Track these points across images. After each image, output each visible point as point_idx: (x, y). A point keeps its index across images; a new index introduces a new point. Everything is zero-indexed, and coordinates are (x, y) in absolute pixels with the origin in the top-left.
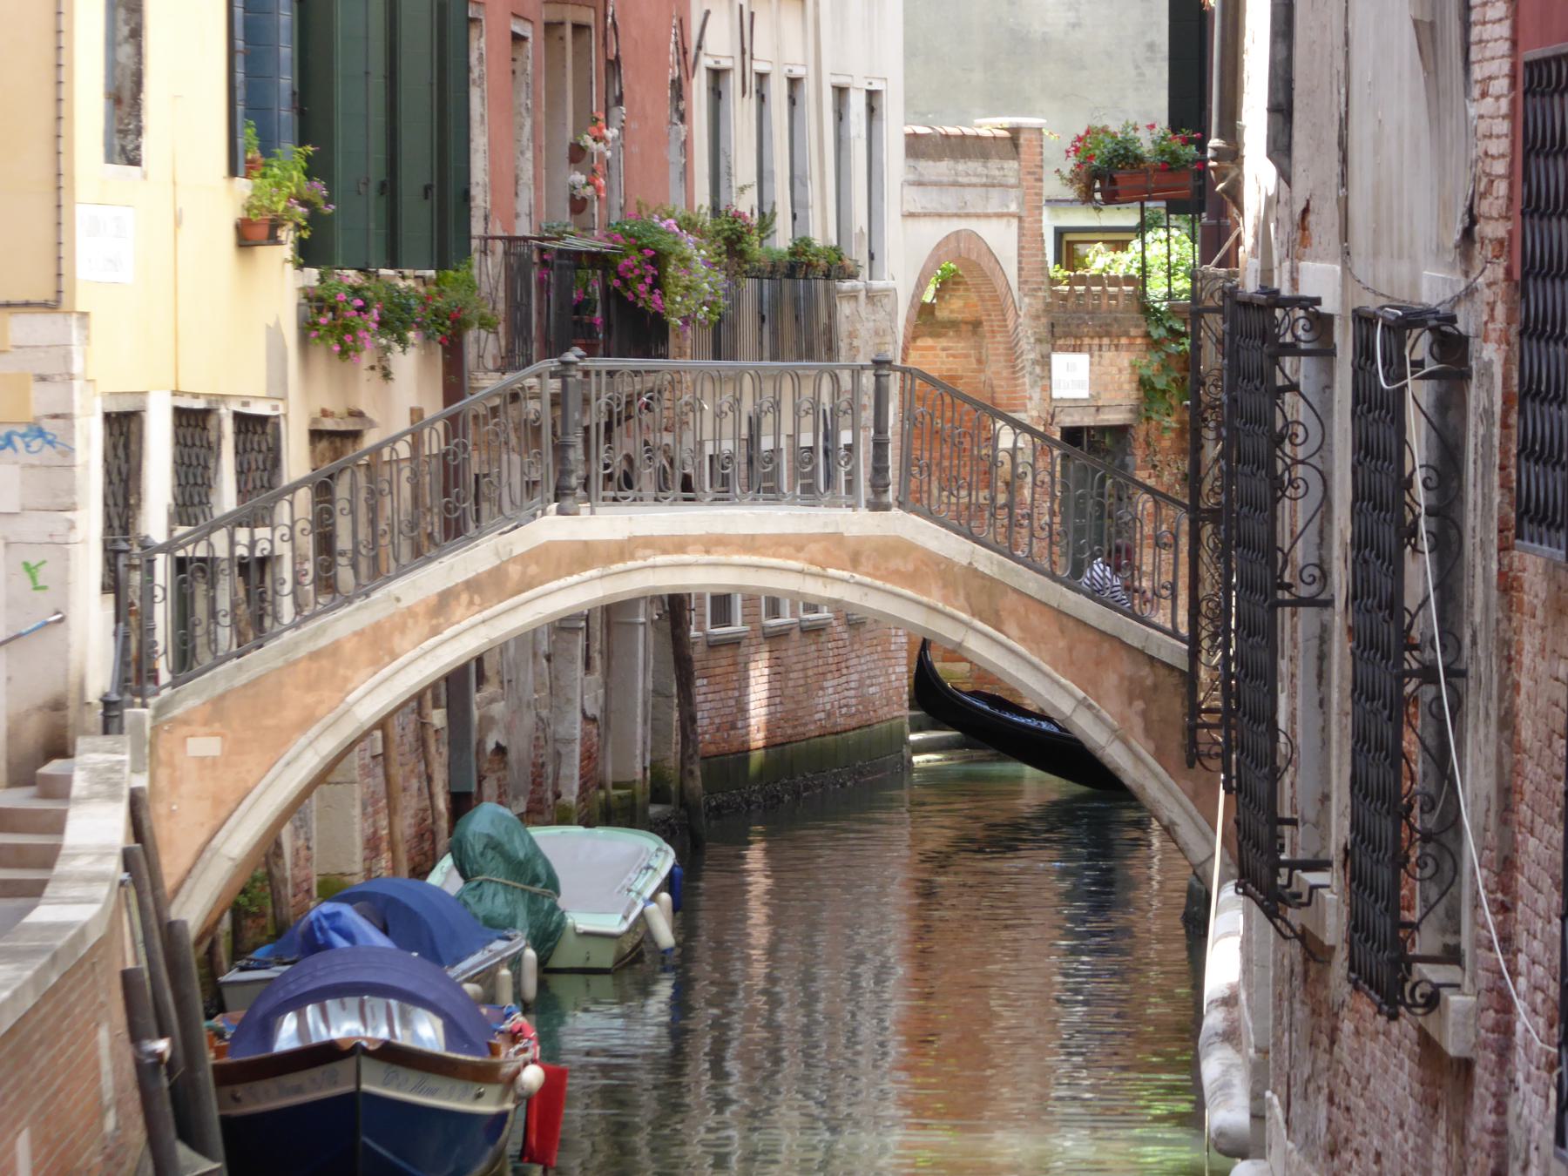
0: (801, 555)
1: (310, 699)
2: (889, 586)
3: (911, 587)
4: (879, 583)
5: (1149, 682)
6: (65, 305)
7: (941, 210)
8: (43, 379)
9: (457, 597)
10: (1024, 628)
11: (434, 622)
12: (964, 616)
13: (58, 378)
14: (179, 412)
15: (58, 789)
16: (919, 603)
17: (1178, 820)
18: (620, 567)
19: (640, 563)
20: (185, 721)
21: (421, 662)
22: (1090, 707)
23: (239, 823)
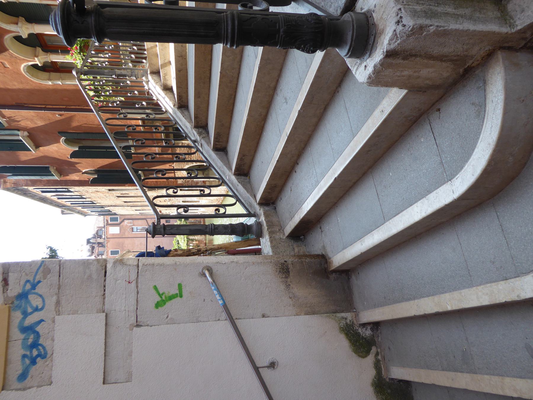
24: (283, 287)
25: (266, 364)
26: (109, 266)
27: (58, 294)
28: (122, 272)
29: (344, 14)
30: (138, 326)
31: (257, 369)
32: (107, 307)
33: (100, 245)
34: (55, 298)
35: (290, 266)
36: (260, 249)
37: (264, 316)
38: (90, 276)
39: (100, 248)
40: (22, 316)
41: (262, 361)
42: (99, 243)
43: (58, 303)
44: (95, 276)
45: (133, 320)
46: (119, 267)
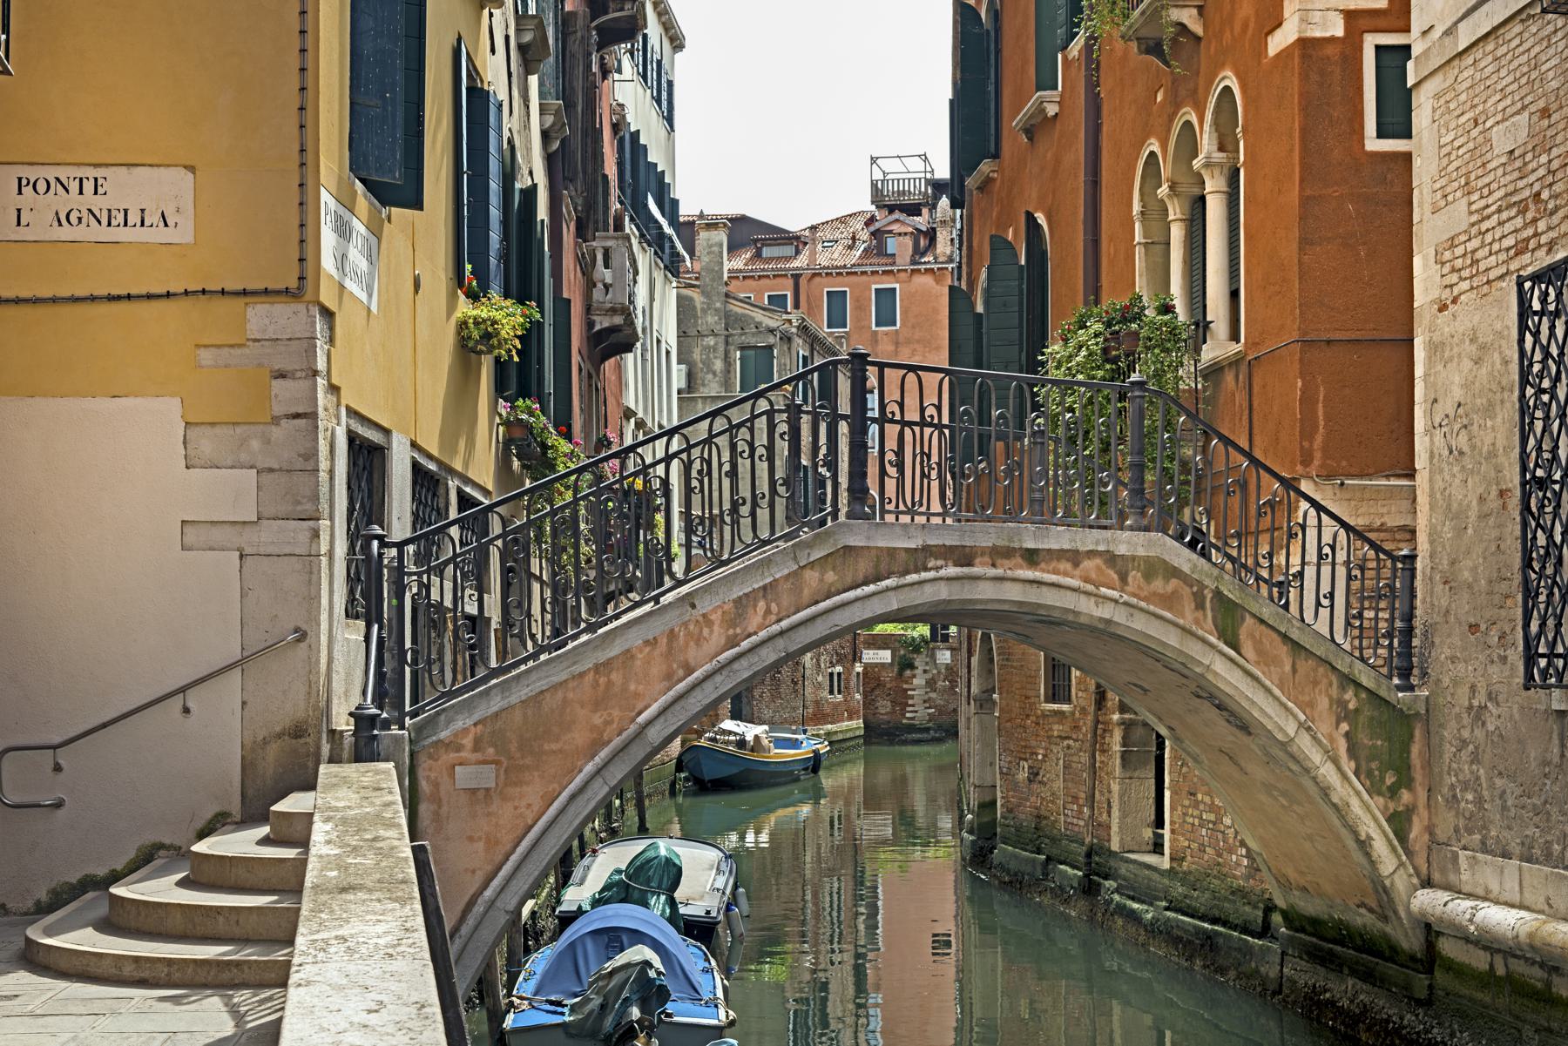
0: (1077, 572)
1: (597, 720)
2: (1152, 608)
3: (1170, 609)
4: (1143, 604)
5: (1351, 706)
6: (309, 296)
7: (682, 703)
8: (282, 375)
9: (756, 601)
10: (1260, 652)
11: (731, 632)
12: (1213, 639)
13: (299, 374)
14: (418, 204)
15: (296, 833)
16: (1176, 625)
17: (1374, 835)
18: (913, 577)
19: (932, 574)
20: (453, 745)
21: (718, 678)
22: (1309, 729)
23: (1005, 601)
24: (278, 729)
25: (190, 704)
26: (311, 523)
27: (280, 470)
28: (304, 537)
29: (607, 902)
30: (241, 556)
31: (183, 690)
32: (265, 522)
33: (923, 242)
34: (276, 466)
35: (302, 741)
36: (1407, 157)
37: (244, 703)
38: (299, 503)
39: (908, 241)
40: (565, 295)
41: (63, 757)
42: (931, 235)
43: (271, 470)
44: (299, 508)
45: (248, 550)
46: (308, 534)
